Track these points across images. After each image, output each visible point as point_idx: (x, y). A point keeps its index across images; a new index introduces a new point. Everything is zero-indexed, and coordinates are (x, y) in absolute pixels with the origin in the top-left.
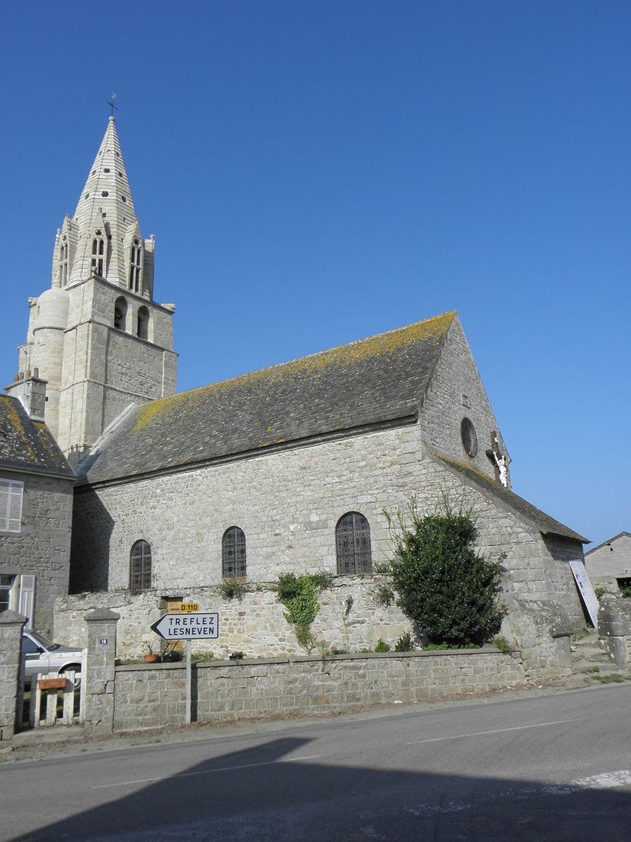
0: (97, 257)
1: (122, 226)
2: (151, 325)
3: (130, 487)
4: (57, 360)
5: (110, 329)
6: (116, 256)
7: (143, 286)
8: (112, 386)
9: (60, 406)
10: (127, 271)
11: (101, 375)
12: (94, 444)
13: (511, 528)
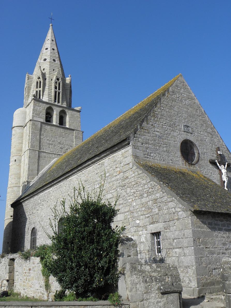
0: (38, 89)
1: (52, 73)
2: (67, 119)
3: (32, 200)
4: (20, 141)
5: (42, 123)
6: (48, 87)
7: (62, 100)
8: (44, 151)
9: (22, 164)
10: (53, 94)
11: (37, 146)
12: (33, 180)
13: (175, 208)
